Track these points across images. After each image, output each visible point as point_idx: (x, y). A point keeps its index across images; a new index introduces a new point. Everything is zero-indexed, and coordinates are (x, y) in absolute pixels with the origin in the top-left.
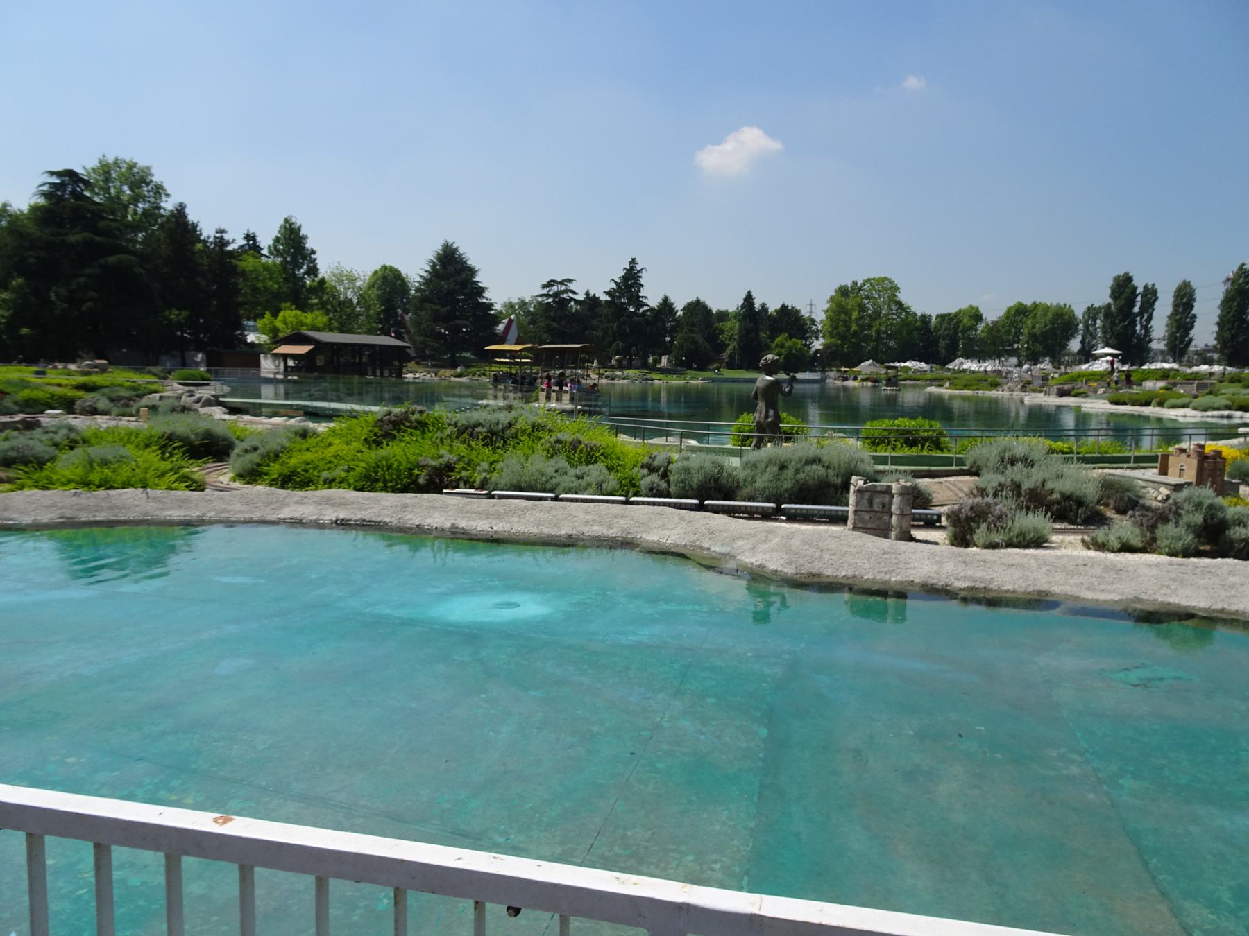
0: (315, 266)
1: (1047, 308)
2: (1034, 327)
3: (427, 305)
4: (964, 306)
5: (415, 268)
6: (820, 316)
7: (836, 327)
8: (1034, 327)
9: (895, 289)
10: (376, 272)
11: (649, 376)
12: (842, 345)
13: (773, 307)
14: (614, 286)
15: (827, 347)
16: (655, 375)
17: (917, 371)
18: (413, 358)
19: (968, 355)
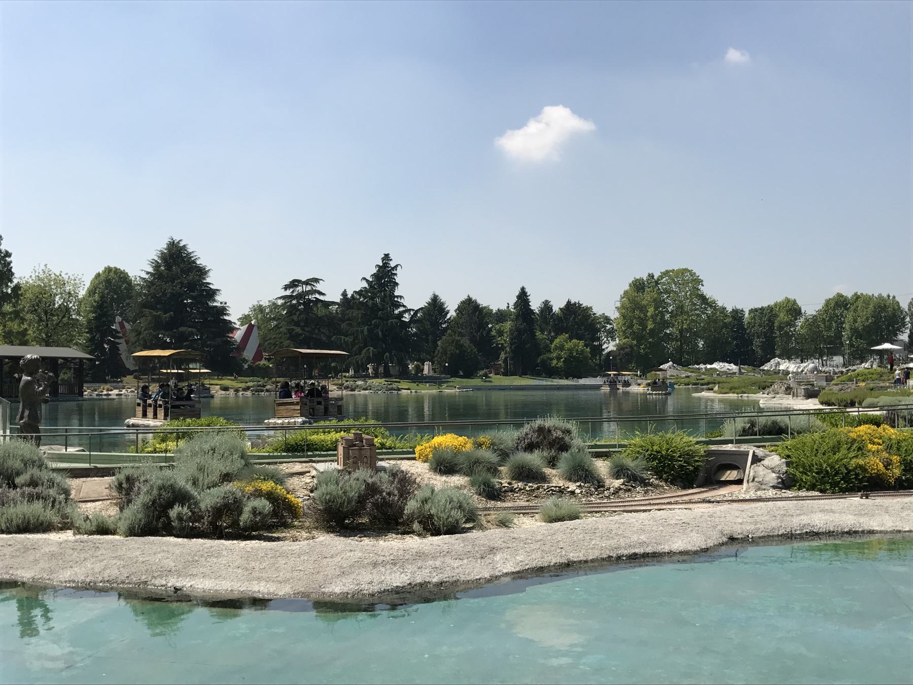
0: (10, 270)
1: (867, 300)
2: (855, 321)
3: (147, 311)
4: (780, 299)
5: (138, 266)
6: (614, 315)
7: (631, 326)
8: (855, 321)
9: (698, 281)
10: (98, 275)
11: (395, 386)
12: (638, 346)
13: (557, 305)
14: (365, 285)
15: (620, 348)
16: (404, 384)
17: (725, 373)
18: (130, 373)
19: (788, 355)
